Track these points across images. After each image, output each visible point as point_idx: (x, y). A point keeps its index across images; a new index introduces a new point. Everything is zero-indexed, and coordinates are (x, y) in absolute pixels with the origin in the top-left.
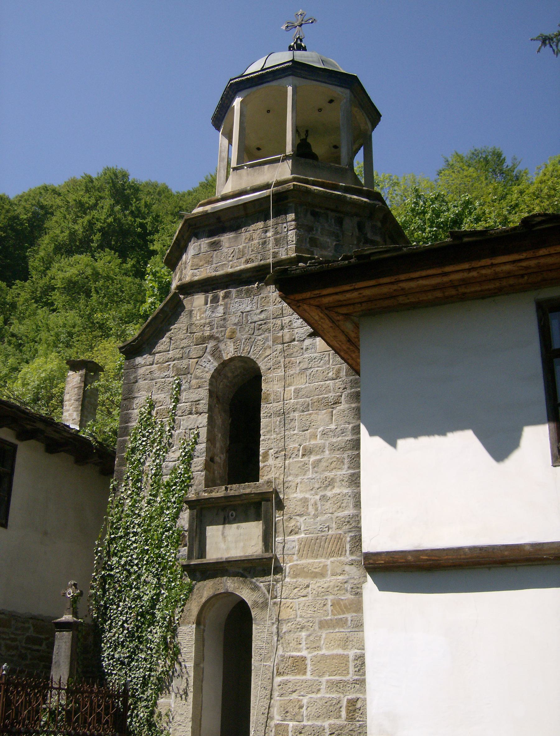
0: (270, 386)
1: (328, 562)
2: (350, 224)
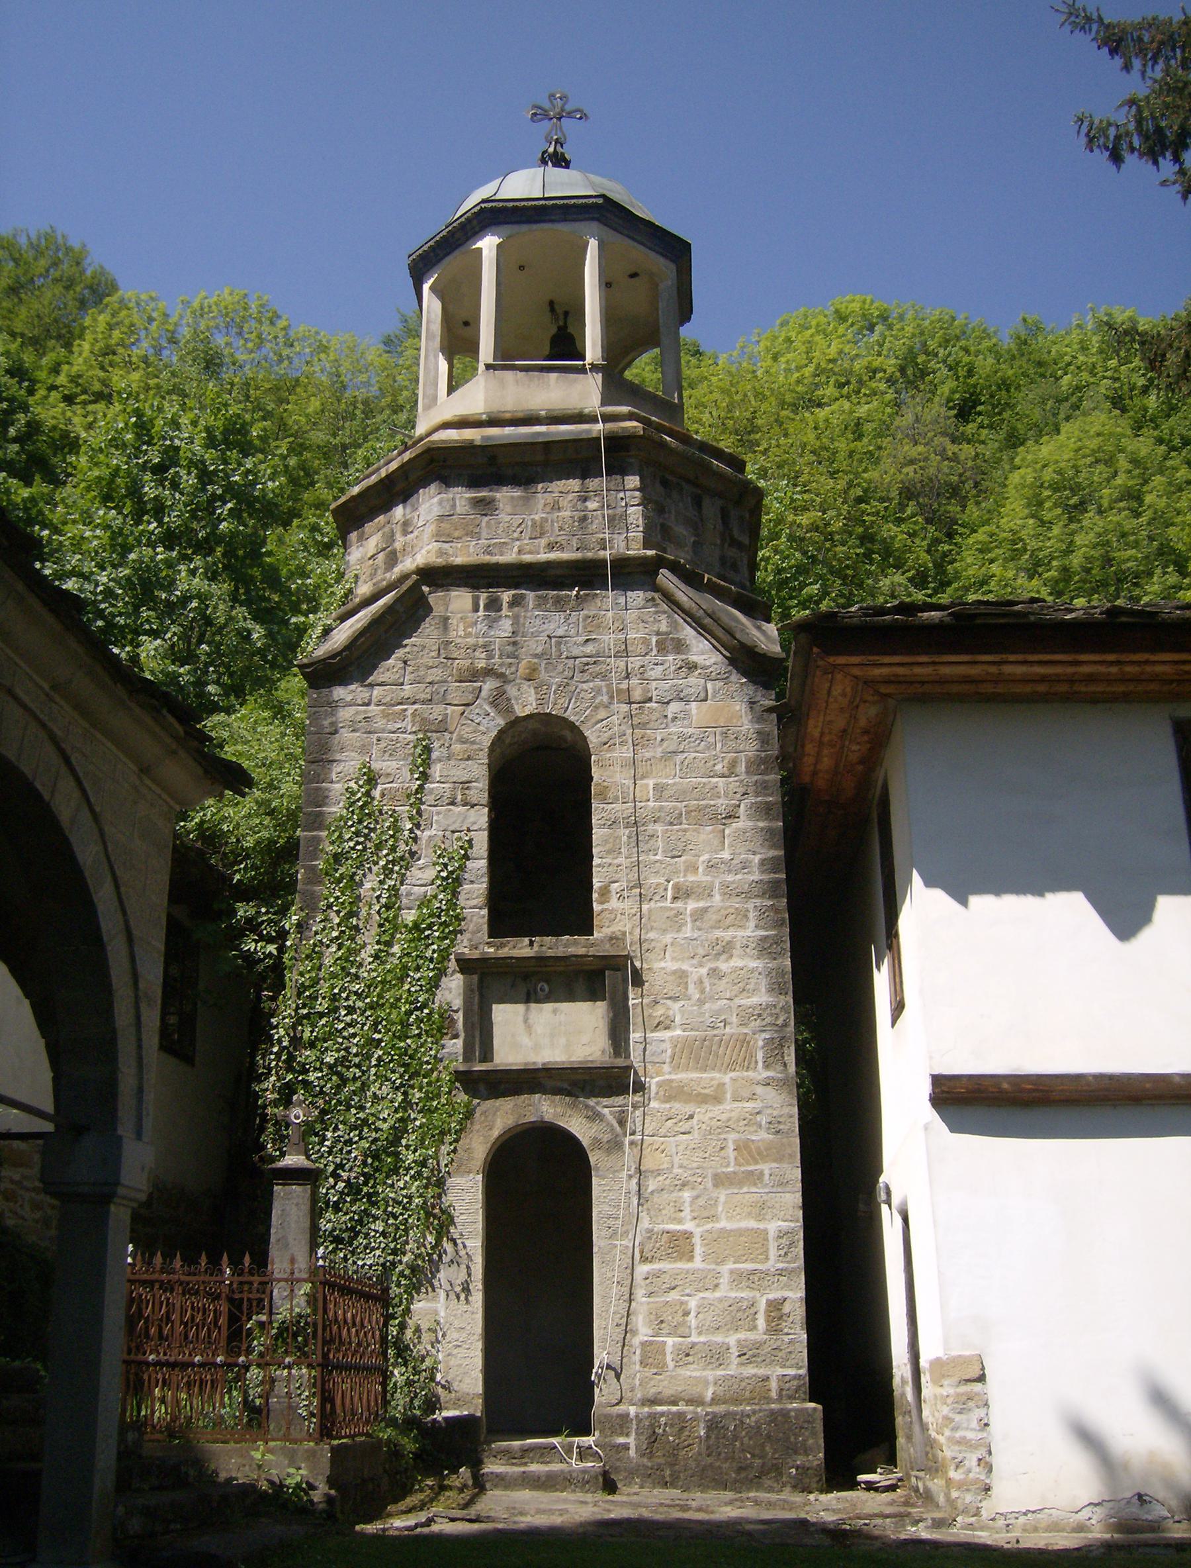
0: (608, 772)
1: (727, 1078)
2: (711, 509)
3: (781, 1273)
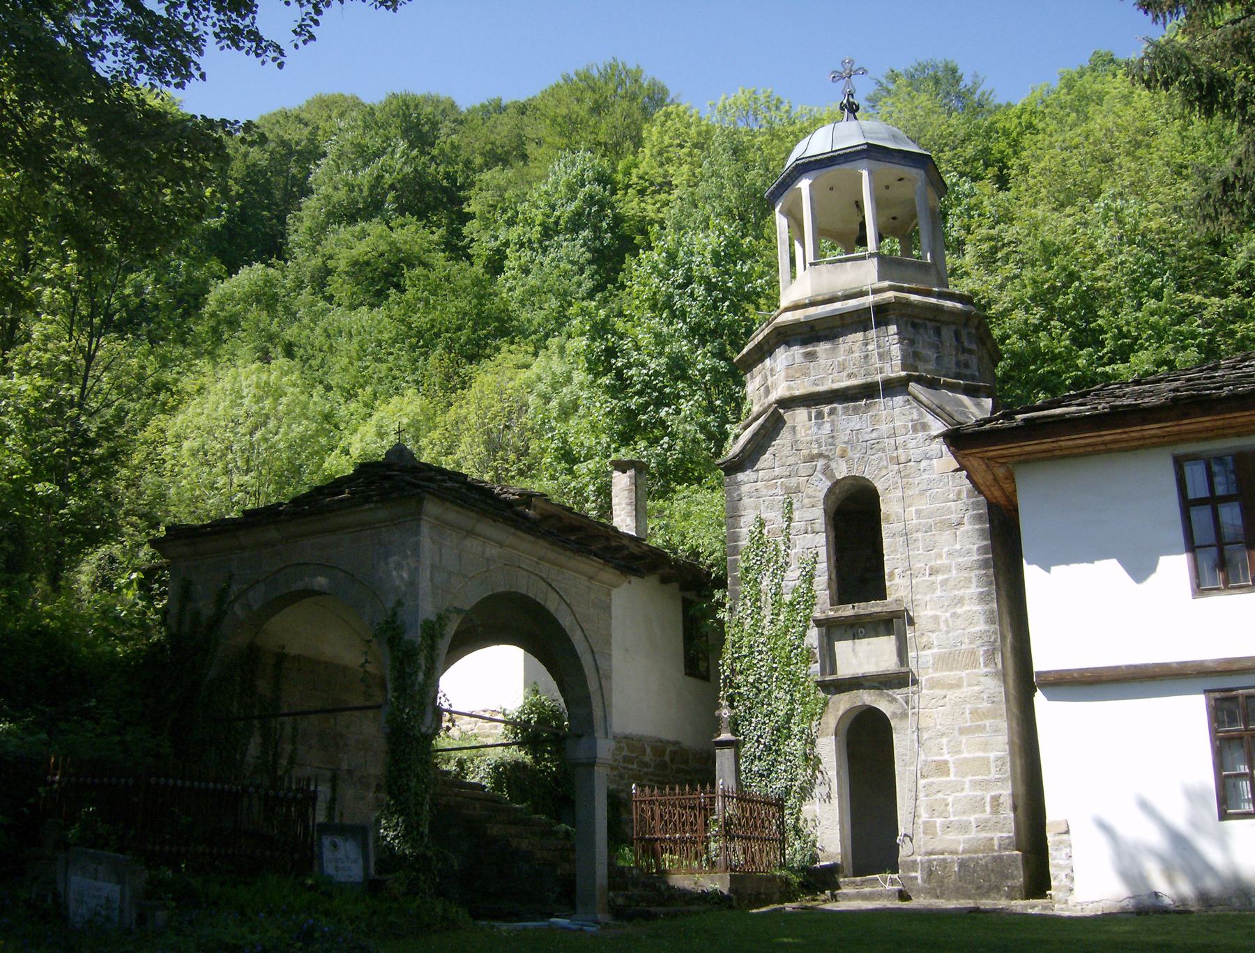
0: (888, 507)
1: (964, 674)
2: (947, 333)
3: (998, 780)
